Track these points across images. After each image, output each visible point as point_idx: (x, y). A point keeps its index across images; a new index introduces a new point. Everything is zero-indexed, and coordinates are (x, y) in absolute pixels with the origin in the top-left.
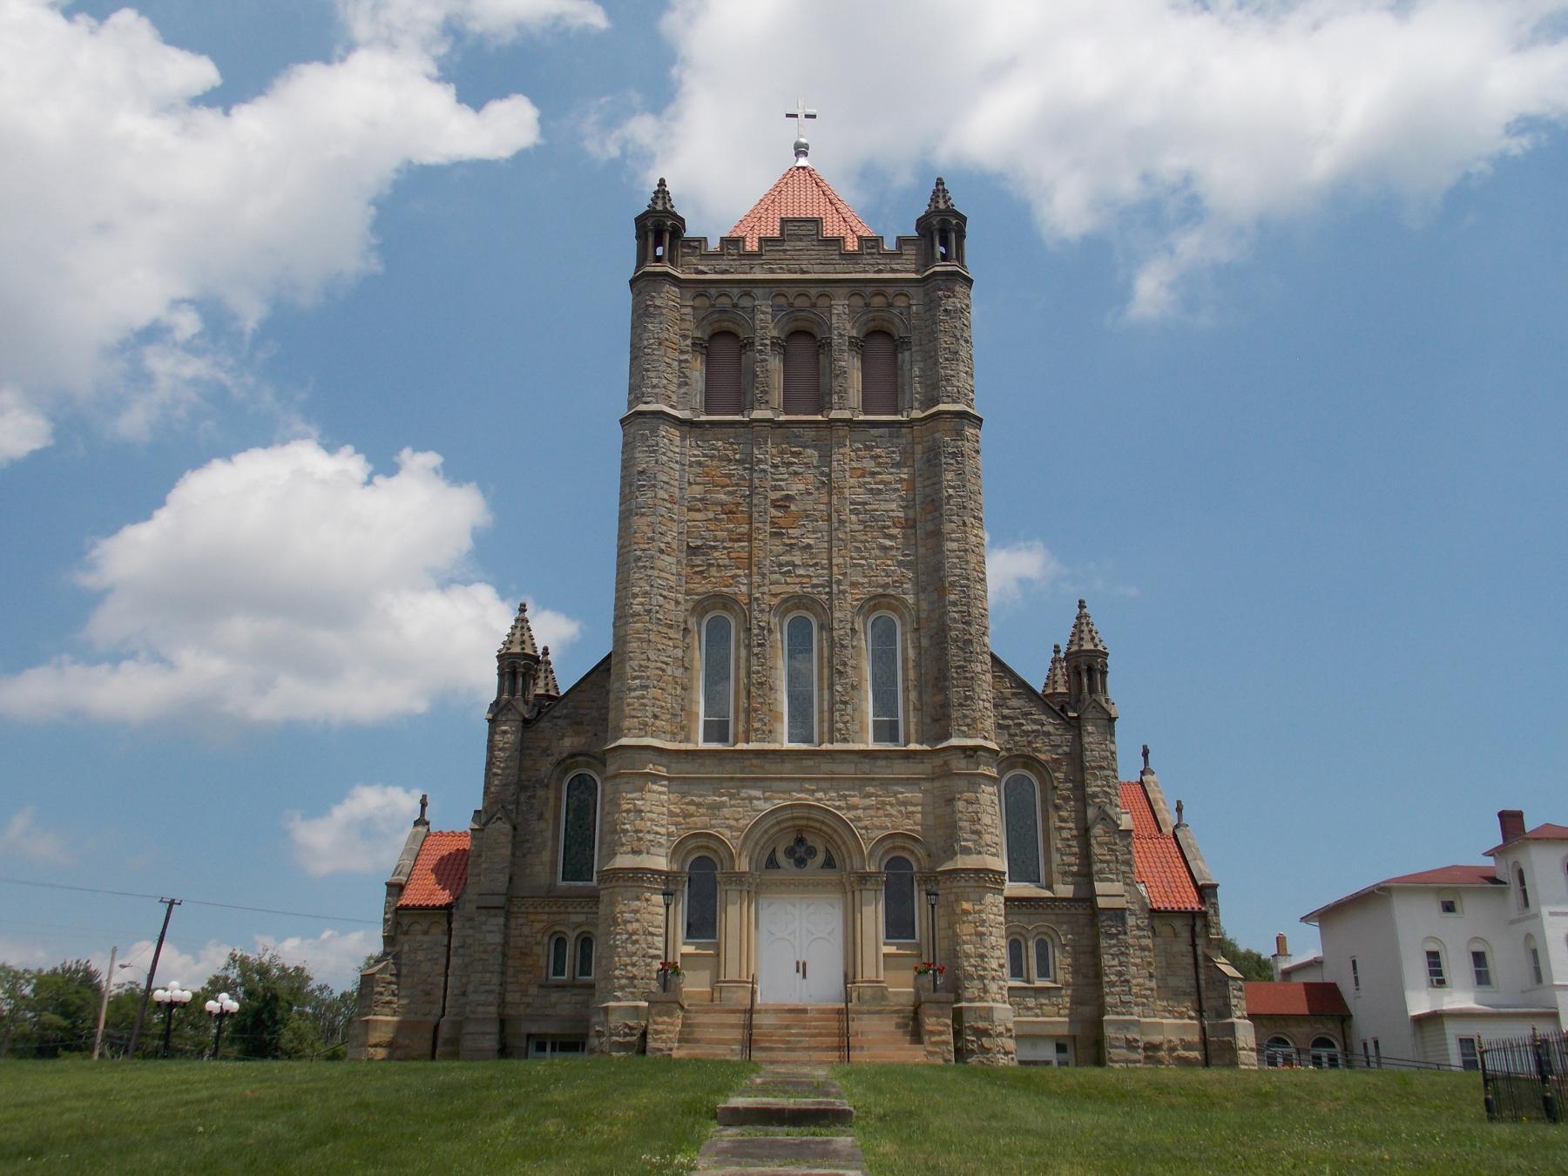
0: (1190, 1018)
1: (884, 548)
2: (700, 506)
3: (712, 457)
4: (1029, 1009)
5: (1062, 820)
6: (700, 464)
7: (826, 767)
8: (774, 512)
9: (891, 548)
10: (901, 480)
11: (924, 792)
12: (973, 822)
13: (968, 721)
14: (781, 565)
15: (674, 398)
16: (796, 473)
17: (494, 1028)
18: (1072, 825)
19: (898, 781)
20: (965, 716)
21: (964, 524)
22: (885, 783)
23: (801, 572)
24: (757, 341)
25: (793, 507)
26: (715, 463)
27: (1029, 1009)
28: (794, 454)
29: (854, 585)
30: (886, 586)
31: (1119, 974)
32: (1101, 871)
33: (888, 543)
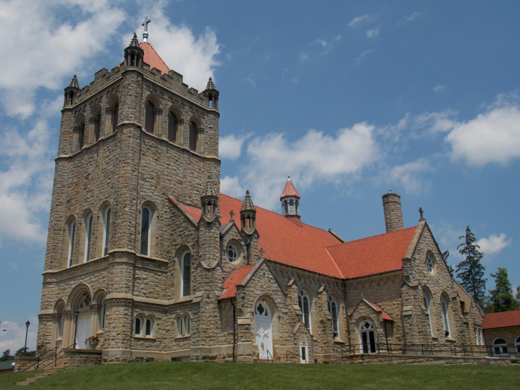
1: (108, 183)
6: (72, 171)
8: (86, 181)
9: (109, 182)
15: (67, 150)
16: (91, 165)
23: (89, 200)
25: (90, 177)
26: (76, 169)
27: (181, 346)
28: (92, 158)
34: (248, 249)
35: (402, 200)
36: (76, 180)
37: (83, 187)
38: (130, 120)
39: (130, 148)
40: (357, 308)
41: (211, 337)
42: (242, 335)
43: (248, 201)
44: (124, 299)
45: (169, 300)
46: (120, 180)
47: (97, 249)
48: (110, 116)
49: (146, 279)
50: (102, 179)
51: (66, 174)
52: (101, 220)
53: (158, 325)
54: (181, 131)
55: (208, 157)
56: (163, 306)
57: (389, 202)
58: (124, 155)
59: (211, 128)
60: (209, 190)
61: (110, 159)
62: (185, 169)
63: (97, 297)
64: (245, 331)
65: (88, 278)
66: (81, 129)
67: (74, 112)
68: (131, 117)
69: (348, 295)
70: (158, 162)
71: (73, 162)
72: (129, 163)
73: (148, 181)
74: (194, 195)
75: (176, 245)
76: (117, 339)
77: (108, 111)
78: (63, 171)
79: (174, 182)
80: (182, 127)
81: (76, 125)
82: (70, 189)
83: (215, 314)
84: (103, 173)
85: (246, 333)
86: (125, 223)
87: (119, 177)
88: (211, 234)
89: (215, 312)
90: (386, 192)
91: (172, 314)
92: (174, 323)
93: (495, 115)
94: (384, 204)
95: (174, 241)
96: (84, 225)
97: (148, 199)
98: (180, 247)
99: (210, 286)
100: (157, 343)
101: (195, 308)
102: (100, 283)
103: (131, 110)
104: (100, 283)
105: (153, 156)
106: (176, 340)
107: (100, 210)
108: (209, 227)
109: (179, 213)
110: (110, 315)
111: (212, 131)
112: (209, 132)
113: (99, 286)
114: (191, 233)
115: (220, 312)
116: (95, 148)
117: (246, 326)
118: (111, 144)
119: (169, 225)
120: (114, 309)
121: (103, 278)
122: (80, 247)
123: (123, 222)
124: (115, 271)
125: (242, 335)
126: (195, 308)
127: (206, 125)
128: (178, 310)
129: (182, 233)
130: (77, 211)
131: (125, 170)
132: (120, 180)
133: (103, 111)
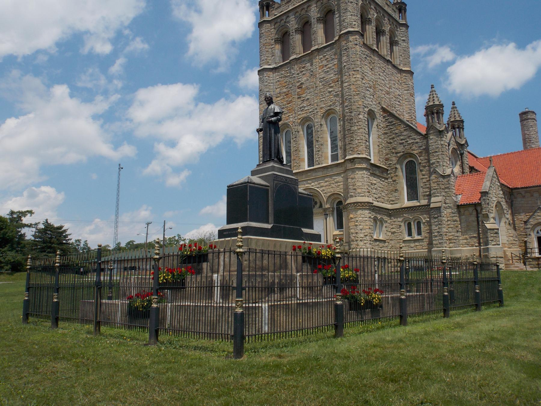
0: (476, 246)
1: (330, 92)
2: (279, 95)
3: (281, 78)
4: (412, 247)
5: (423, 175)
6: (278, 81)
7: (314, 174)
8: (298, 90)
9: (332, 91)
10: (335, 64)
11: (342, 177)
12: (354, 185)
13: (352, 149)
14: (301, 108)
15: (270, 62)
16: (304, 74)
17: (478, 252)
18: (426, 177)
19: (334, 175)
20: (351, 147)
21: (350, 75)
22: (331, 176)
23: (306, 108)
24: (291, 32)
25: (303, 87)
26: (283, 79)
27: (412, 247)
28: (303, 67)
29: (321, 108)
30: (330, 106)
31: (438, 232)
32: (434, 193)
33: (331, 90)
34: (461, 157)
35: (537, 117)
36: (285, 90)
37: (296, 97)
38: (353, 28)
39: (358, 56)
40: (533, 215)
41: (450, 239)
42: (492, 238)
43: (456, 112)
44: (368, 203)
45: (392, 204)
46: (352, 87)
47: (323, 155)
48: (321, 26)
49: (375, 184)
50: (321, 87)
51: (272, 84)
52: (325, 128)
53: (386, 227)
54: (383, 42)
55: (404, 69)
56: (388, 209)
57: (528, 119)
58: (353, 63)
59: (403, 40)
60: (436, 99)
61: (329, 68)
62: (390, 80)
63: (330, 200)
64: (495, 235)
65: (316, 183)
66: (283, 39)
67: (273, 24)
68: (355, 25)
69: (514, 202)
70: (373, 72)
71: (278, 72)
72: (358, 71)
73: (368, 90)
74: (397, 106)
75: (397, 153)
76: (365, 240)
77: (319, 20)
78: (269, 81)
79: (384, 93)
80: (384, 38)
81: (277, 37)
82: (279, 99)
83: (455, 218)
84: (321, 82)
85: (495, 237)
86: (361, 130)
87: (350, 85)
88: (442, 143)
89: (455, 216)
90: (524, 110)
91: (397, 218)
92: (400, 226)
93: (494, 50)
94: (521, 121)
95: (394, 148)
96: (301, 133)
97: (370, 108)
98: (403, 155)
99: (446, 192)
100: (387, 244)
101: (434, 213)
102: (332, 187)
103: (353, 18)
104: (332, 187)
105: (369, 65)
106: (405, 241)
107: (322, 118)
108: (440, 135)
109: (398, 122)
110: (356, 217)
111: (405, 44)
112: (402, 44)
113: (332, 190)
114: (416, 141)
115: (460, 217)
116: (308, 58)
117: (496, 231)
118: (329, 53)
119: (386, 133)
120: (360, 212)
121: (336, 183)
122: (300, 153)
123: (359, 129)
124: (356, 176)
125: (492, 238)
126: (434, 213)
127: (400, 37)
128: (405, 214)
129: (403, 141)
130: (291, 119)
131: (355, 78)
132: (352, 87)
133: (313, 21)
